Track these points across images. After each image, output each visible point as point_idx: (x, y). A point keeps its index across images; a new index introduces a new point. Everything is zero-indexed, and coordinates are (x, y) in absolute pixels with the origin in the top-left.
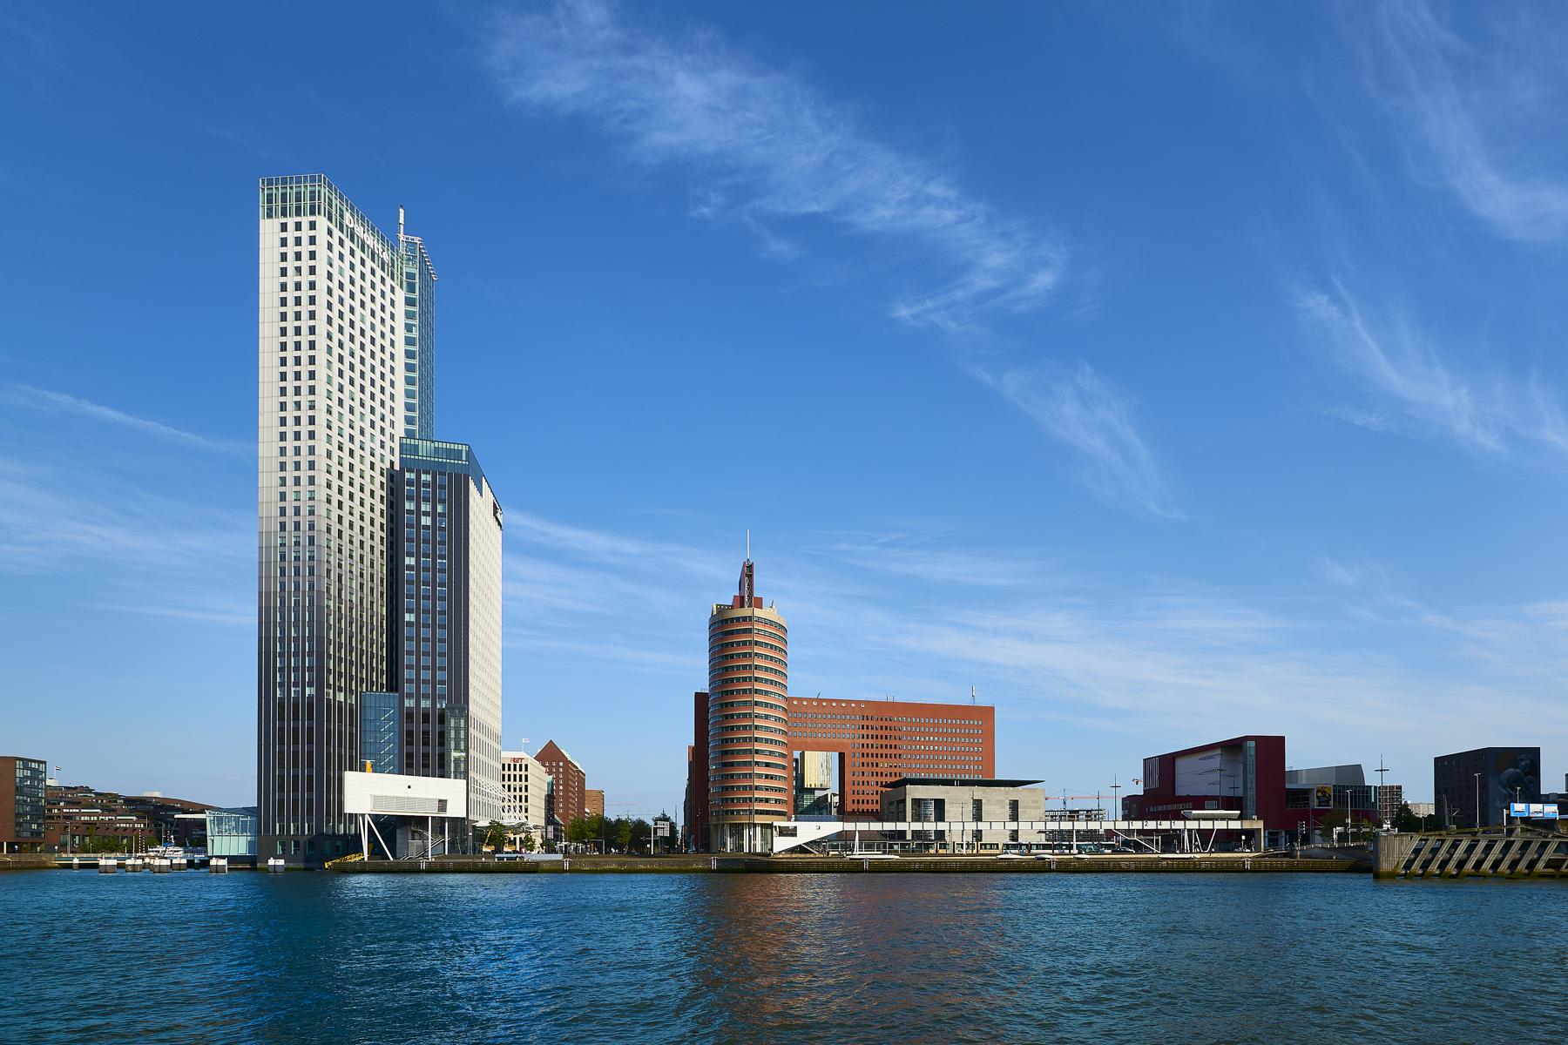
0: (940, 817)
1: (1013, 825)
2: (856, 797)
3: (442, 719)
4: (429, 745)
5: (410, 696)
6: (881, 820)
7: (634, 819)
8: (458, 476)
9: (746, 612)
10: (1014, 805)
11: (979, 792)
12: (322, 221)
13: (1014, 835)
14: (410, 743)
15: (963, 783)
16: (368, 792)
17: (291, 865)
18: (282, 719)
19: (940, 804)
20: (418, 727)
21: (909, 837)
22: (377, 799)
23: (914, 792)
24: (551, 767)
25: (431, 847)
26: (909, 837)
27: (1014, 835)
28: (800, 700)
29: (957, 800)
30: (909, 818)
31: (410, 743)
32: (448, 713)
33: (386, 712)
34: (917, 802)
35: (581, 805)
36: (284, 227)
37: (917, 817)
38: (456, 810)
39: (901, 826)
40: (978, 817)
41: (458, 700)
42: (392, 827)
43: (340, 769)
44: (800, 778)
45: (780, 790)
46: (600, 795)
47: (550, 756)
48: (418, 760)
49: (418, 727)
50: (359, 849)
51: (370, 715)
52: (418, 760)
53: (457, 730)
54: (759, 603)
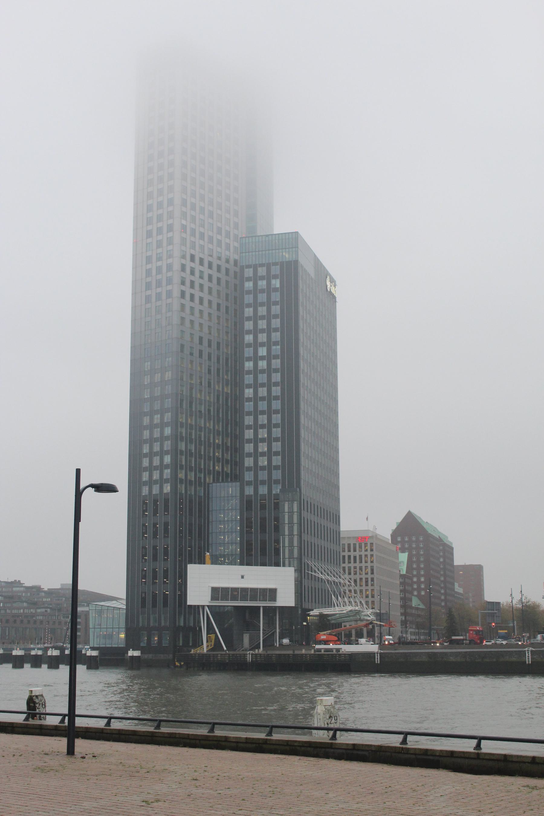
16: (203, 583)
22: (216, 593)
38: (286, 598)
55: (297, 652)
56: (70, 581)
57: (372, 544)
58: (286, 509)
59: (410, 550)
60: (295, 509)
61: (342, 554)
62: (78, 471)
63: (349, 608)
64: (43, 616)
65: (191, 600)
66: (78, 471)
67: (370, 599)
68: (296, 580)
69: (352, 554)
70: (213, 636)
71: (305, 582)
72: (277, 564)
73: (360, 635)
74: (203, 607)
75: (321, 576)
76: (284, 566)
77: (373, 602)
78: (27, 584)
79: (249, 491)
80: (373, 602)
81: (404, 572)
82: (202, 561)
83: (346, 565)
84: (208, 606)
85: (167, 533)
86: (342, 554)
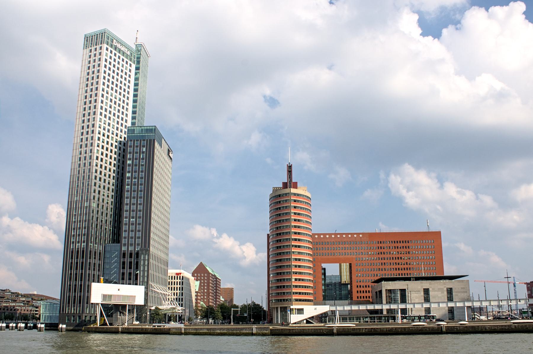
0: (404, 300)
1: (426, 305)
2: (359, 289)
3: (137, 254)
4: (131, 269)
5: (125, 245)
6: (372, 303)
7: (250, 302)
8: (150, 140)
9: (287, 191)
10: (450, 291)
11: (426, 284)
12: (105, 46)
13: (428, 310)
14: (123, 268)
15: (417, 279)
16: (100, 292)
17: (69, 328)
18: (72, 258)
19: (403, 291)
20: (127, 260)
21: (385, 313)
22: (105, 297)
23: (387, 286)
24: (197, 276)
25: (126, 320)
26: (385, 313)
27: (428, 310)
28: (319, 235)
29: (415, 290)
30: (384, 301)
31: (123, 268)
32: (140, 252)
33: (114, 253)
34: (390, 291)
35: (216, 297)
36: (91, 51)
37: (389, 302)
38: (140, 301)
39: (378, 307)
40: (427, 299)
41: (145, 246)
42: (112, 309)
43: (89, 280)
44: (147, 288)
45: (308, 287)
46: (231, 291)
47: (200, 272)
48: (126, 276)
49: (127, 260)
50: (95, 321)
51: (108, 255)
52: (126, 276)
53: (144, 260)
54: (295, 186)
55: (143, 327)
56: (446, 274)
57: (183, 277)
58: (142, 258)
59: (200, 280)
60: (146, 258)
61: (168, 281)
62: (290, 167)
63: (171, 306)
64: (358, 318)
65: (93, 300)
66: (290, 167)
67: (181, 302)
68: (145, 292)
69: (173, 281)
70: (103, 319)
71: (150, 293)
72: (136, 284)
73: (170, 320)
74: (98, 304)
75: (157, 290)
76: (140, 285)
77: (182, 304)
78: (12, 291)
79: (123, 249)
80: (182, 304)
81: (197, 290)
82: (99, 281)
83: (170, 286)
84: (102, 304)
85: (78, 268)
86: (168, 281)
